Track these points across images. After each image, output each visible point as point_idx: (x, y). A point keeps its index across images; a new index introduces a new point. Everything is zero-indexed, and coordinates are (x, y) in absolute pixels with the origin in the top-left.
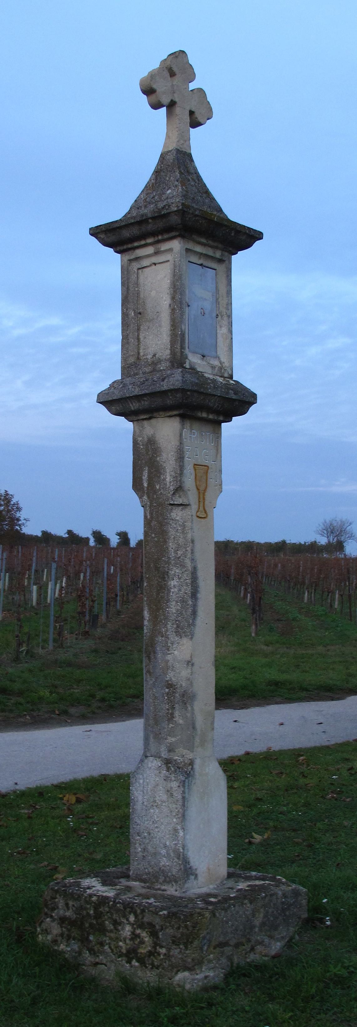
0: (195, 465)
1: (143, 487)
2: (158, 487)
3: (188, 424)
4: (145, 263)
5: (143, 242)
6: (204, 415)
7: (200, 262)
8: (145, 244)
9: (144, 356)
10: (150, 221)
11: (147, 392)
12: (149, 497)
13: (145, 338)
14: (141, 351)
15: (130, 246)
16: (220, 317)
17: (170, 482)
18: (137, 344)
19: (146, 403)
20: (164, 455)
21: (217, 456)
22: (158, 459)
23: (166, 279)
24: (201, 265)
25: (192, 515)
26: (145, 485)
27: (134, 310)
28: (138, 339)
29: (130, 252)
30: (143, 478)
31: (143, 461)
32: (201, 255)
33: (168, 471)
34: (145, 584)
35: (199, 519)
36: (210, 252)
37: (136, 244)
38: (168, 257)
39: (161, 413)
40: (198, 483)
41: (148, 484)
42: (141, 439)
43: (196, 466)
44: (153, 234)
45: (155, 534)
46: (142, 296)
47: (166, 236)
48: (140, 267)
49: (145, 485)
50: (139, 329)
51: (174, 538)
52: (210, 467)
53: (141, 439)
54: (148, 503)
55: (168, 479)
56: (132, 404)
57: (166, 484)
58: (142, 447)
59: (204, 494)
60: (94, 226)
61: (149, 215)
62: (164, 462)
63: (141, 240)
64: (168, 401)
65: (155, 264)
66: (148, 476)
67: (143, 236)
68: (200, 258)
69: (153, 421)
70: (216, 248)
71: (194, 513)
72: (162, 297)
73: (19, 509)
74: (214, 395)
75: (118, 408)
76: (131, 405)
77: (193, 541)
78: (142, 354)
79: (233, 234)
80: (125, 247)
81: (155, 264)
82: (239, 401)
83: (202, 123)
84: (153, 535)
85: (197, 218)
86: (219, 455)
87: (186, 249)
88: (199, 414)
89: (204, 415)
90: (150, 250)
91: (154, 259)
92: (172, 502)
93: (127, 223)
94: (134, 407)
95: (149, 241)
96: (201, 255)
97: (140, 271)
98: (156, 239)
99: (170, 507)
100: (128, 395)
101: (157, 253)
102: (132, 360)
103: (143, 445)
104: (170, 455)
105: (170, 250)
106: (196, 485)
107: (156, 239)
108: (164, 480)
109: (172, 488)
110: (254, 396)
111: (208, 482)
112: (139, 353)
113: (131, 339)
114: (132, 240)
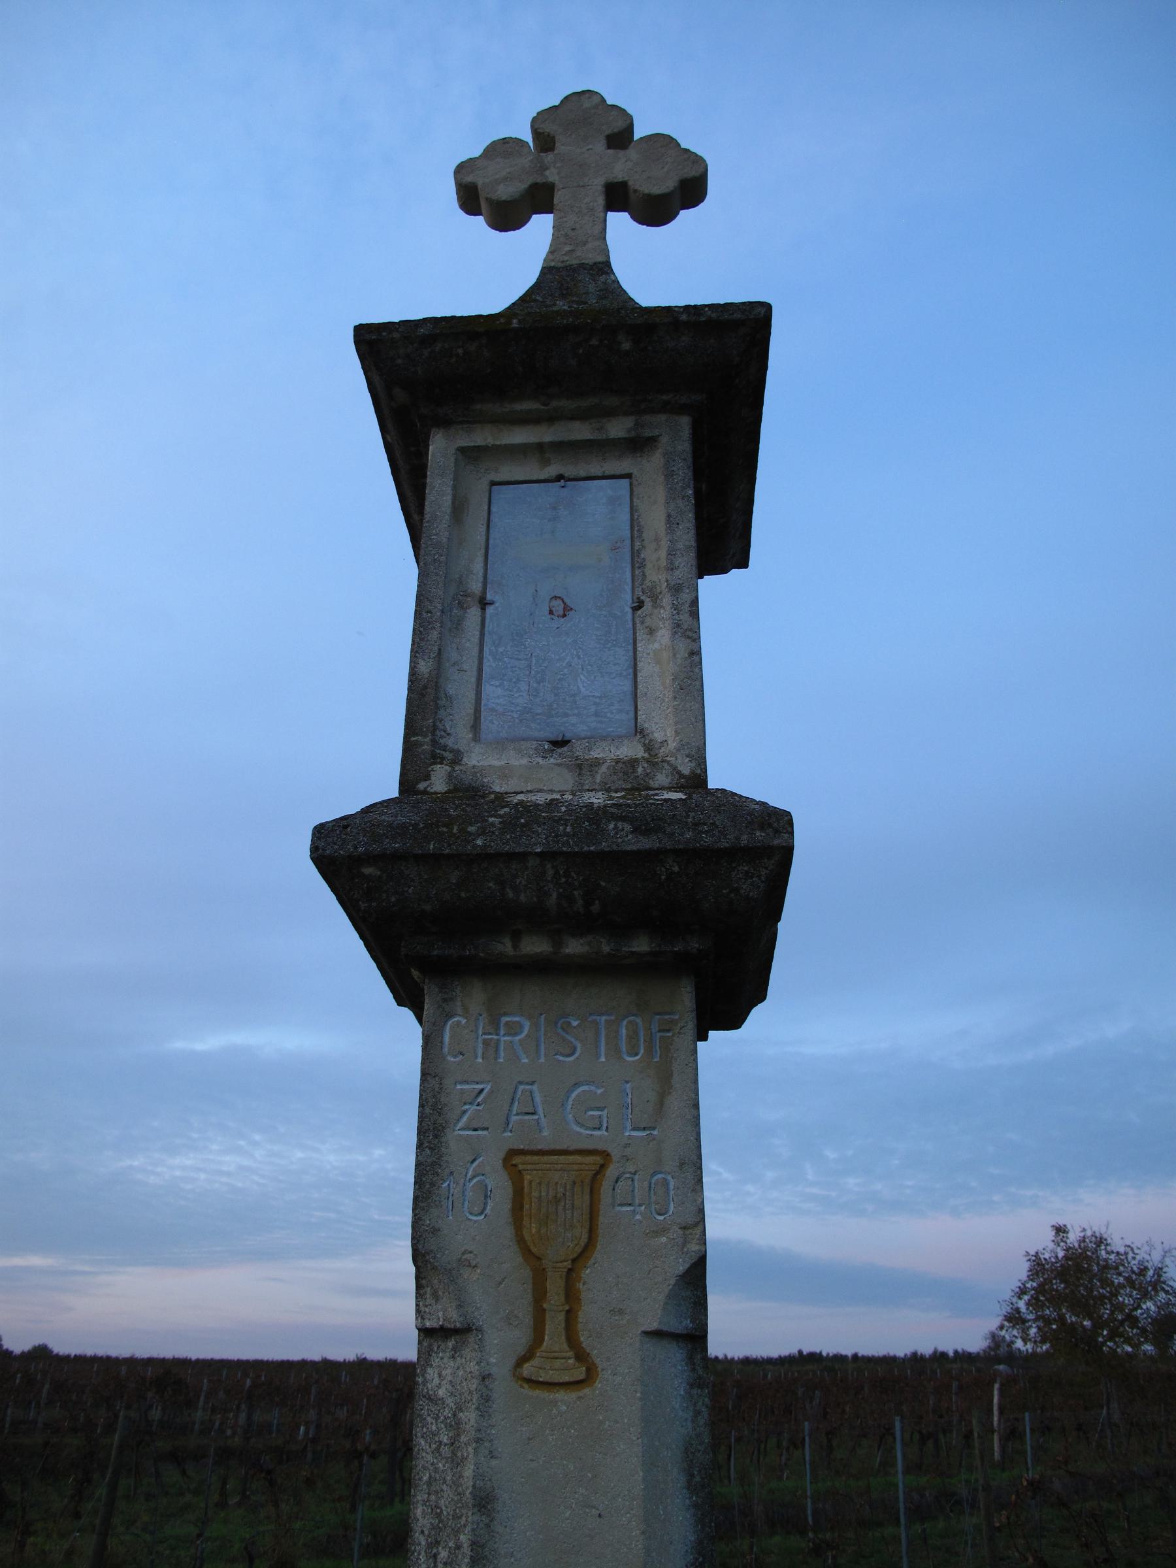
0: (512, 1153)
3: (473, 999)
6: (535, 946)
7: (552, 470)
16: (648, 604)
21: (661, 1103)
24: (559, 478)
25: (485, 1377)
32: (541, 451)
35: (527, 1391)
36: (581, 431)
40: (531, 1229)
43: (517, 1160)
51: (429, 1483)
52: (615, 1154)
59: (571, 1276)
68: (546, 462)
70: (610, 413)
71: (499, 1361)
74: (523, 857)
77: (484, 1502)
79: (626, 346)
82: (687, 854)
83: (702, 170)
85: (438, 347)
86: (675, 1103)
87: (462, 450)
88: (505, 947)
89: (535, 946)
96: (541, 451)
106: (520, 1240)
110: (778, 822)
111: (602, 1220)
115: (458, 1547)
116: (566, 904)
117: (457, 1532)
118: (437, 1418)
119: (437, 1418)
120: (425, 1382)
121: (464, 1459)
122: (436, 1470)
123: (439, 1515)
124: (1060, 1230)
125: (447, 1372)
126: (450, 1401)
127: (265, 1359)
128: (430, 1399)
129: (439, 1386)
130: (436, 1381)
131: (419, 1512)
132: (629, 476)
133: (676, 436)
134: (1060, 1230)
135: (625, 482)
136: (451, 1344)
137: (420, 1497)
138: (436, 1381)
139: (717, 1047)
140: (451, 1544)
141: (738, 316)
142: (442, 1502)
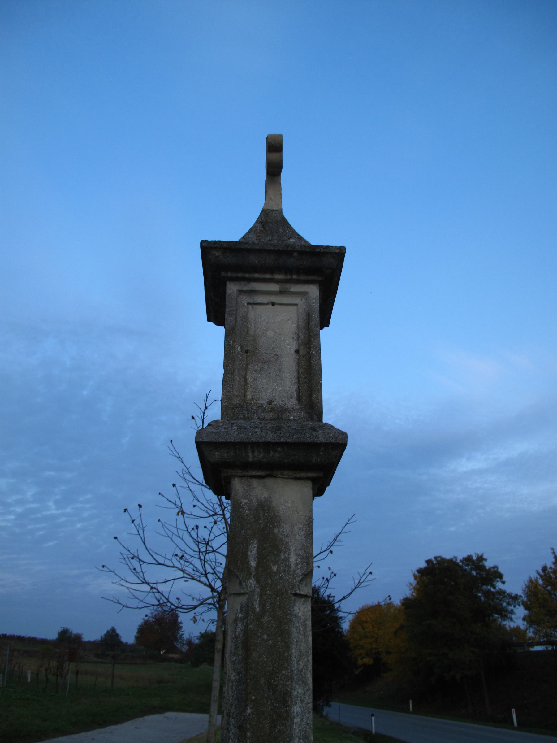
1: (248, 567)
2: (275, 569)
4: (260, 299)
5: (268, 276)
8: (270, 279)
9: (252, 400)
10: (295, 254)
11: (289, 440)
12: (258, 581)
13: (255, 379)
14: (248, 393)
15: (247, 275)
17: (297, 564)
18: (244, 384)
19: (277, 455)
20: (286, 528)
22: (276, 531)
23: (290, 322)
26: (253, 564)
27: (240, 345)
28: (246, 380)
29: (242, 283)
30: (249, 553)
31: (250, 532)
33: (293, 549)
34: (249, 711)
37: (257, 275)
38: (297, 300)
39: (286, 472)
41: (258, 564)
42: (246, 501)
44: (287, 270)
45: (268, 635)
46: (251, 332)
47: (303, 277)
48: (251, 301)
49: (253, 564)
50: (246, 368)
51: (297, 642)
53: (246, 501)
54: (258, 590)
55: (293, 559)
56: (253, 452)
57: (290, 567)
58: (247, 512)
60: (210, 238)
61: (298, 248)
62: (287, 536)
63: (266, 273)
64: (315, 458)
65: (273, 304)
66: (258, 552)
67: (272, 270)
69: (269, 482)
72: (284, 340)
73: (486, 560)
75: (225, 455)
76: (250, 454)
78: (249, 397)
80: (240, 275)
81: (273, 304)
84: (265, 637)
90: (275, 287)
91: (274, 299)
92: (298, 592)
93: (262, 248)
94: (254, 457)
95: (277, 277)
97: (250, 306)
98: (289, 277)
99: (293, 598)
100: (254, 440)
101: (281, 293)
102: (236, 401)
103: (249, 510)
104: (296, 528)
105: (304, 294)
107: (289, 277)
108: (287, 559)
109: (299, 572)
112: (245, 396)
113: (236, 377)
114: (255, 269)
115: (308, 661)
116: (268, 449)
117: (307, 657)
118: (298, 622)
119: (298, 622)
120: (294, 610)
121: (308, 635)
122: (299, 638)
123: (301, 652)
124: (200, 633)
125: (302, 609)
126: (303, 617)
127: (48, 639)
128: (295, 616)
129: (299, 613)
130: (298, 611)
131: (293, 651)
132: (296, 305)
133: (314, 291)
134: (200, 633)
135: (295, 307)
136: (303, 600)
137: (294, 646)
138: (298, 611)
139: (318, 499)
140: (306, 660)
141: (337, 251)
142: (301, 648)
